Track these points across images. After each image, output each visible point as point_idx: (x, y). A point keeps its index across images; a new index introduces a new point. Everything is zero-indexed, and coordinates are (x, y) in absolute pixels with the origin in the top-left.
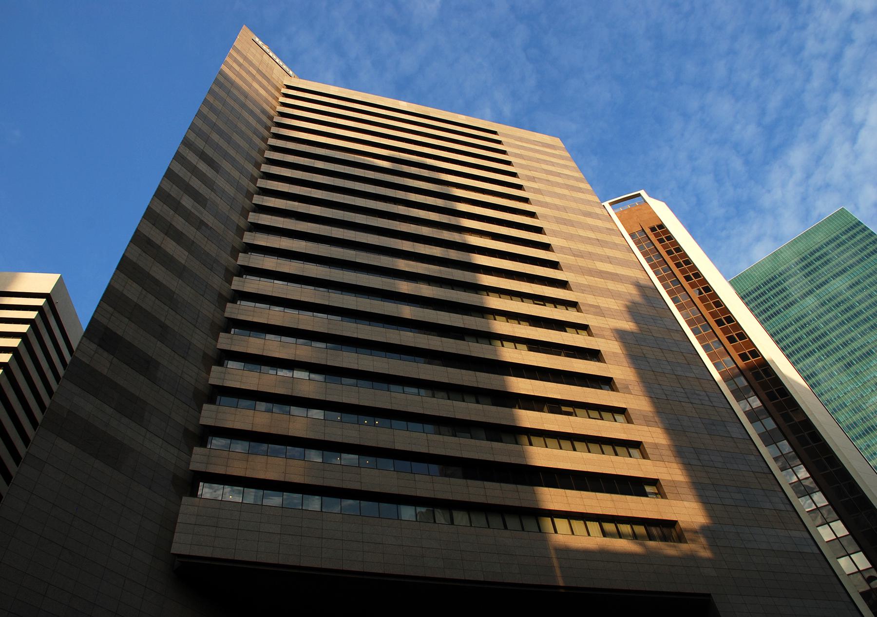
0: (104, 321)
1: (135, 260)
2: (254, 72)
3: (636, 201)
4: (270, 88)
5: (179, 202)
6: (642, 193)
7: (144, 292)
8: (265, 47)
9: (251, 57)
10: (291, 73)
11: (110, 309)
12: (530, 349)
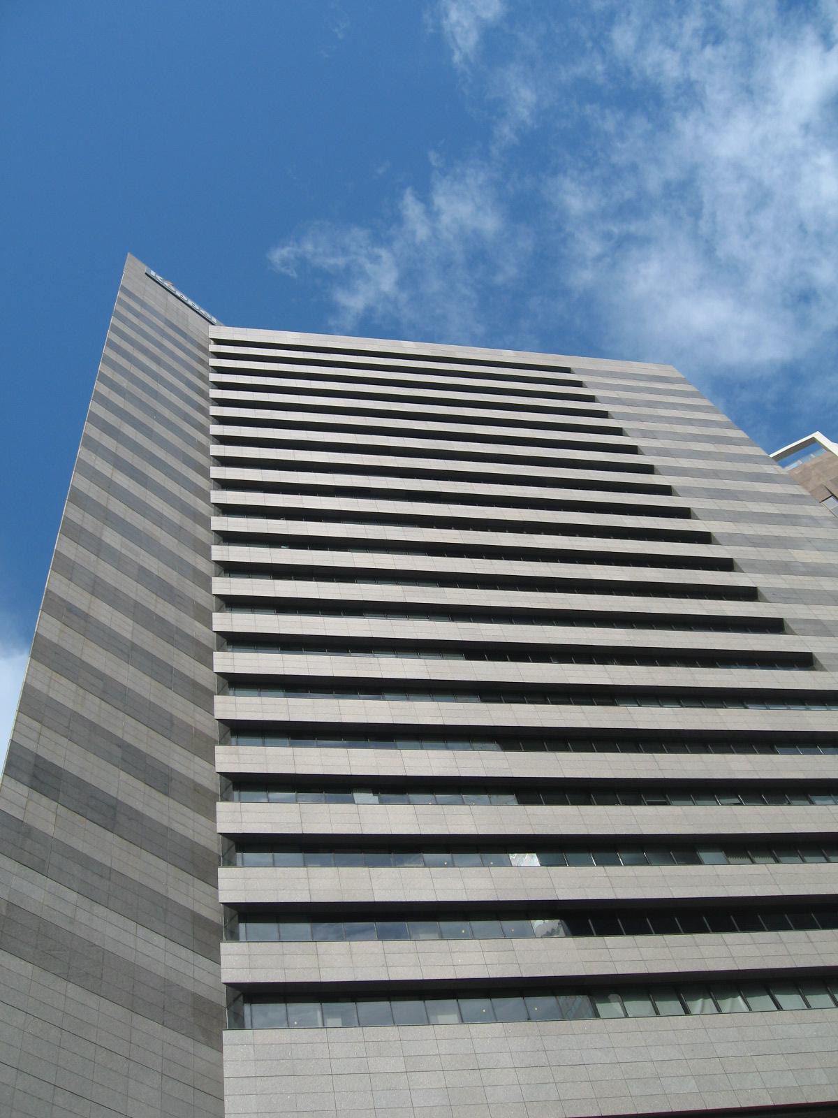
0: (31, 745)
1: (55, 640)
2: (161, 325)
3: (813, 458)
4: (189, 346)
5: (100, 539)
6: (818, 436)
7: (81, 691)
8: (167, 284)
9: (151, 302)
10: (214, 320)
11: (36, 725)
12: (523, 801)
